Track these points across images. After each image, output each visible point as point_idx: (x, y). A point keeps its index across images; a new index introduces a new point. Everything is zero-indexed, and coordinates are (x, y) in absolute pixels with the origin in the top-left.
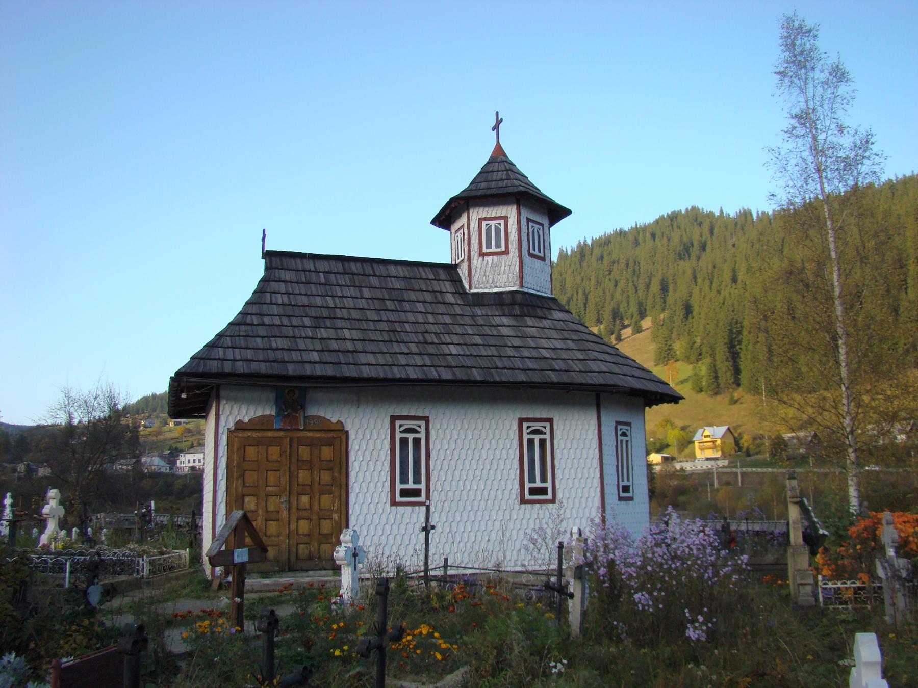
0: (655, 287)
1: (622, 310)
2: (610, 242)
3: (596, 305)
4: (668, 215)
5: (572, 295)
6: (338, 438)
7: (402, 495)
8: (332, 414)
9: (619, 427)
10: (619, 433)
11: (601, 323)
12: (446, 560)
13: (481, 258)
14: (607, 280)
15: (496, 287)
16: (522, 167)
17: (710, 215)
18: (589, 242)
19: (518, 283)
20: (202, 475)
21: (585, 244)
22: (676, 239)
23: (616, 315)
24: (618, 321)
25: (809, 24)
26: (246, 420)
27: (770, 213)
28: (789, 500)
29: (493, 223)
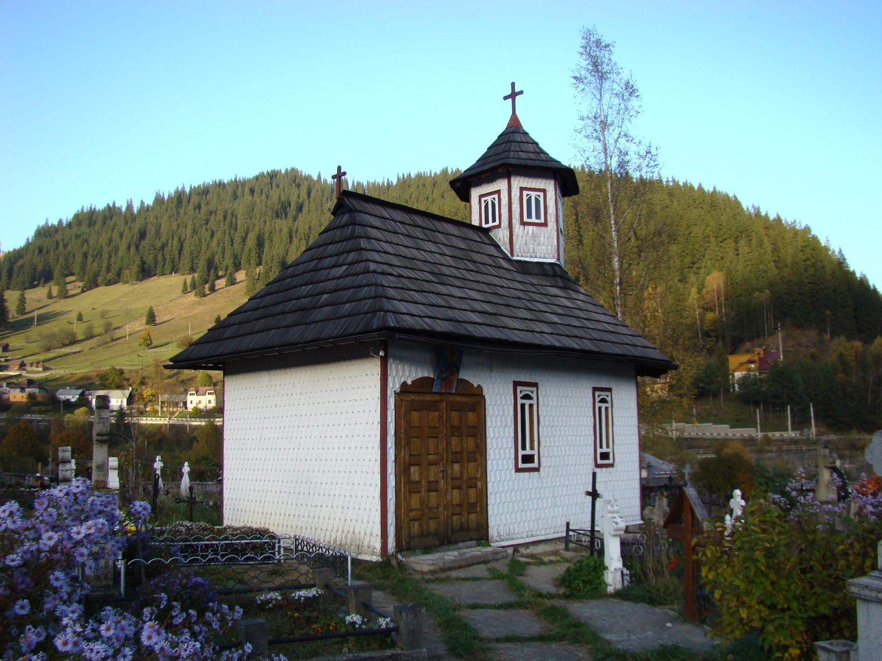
0: (251, 242)
1: (216, 261)
2: (208, 192)
3: (191, 253)
4: (268, 172)
5: (167, 241)
6: (475, 402)
7: (523, 462)
8: (473, 377)
9: (519, 389)
10: (597, 399)
11: (195, 271)
12: (568, 524)
13: (522, 227)
14: (204, 230)
15: (536, 257)
16: (534, 135)
17: (308, 178)
18: (188, 190)
19: (556, 255)
20: (222, 434)
21: (183, 192)
22: (274, 198)
23: (211, 265)
24: (212, 271)
25: (606, 40)
26: (409, 382)
27: (365, 184)
28: (95, 437)
29: (533, 194)
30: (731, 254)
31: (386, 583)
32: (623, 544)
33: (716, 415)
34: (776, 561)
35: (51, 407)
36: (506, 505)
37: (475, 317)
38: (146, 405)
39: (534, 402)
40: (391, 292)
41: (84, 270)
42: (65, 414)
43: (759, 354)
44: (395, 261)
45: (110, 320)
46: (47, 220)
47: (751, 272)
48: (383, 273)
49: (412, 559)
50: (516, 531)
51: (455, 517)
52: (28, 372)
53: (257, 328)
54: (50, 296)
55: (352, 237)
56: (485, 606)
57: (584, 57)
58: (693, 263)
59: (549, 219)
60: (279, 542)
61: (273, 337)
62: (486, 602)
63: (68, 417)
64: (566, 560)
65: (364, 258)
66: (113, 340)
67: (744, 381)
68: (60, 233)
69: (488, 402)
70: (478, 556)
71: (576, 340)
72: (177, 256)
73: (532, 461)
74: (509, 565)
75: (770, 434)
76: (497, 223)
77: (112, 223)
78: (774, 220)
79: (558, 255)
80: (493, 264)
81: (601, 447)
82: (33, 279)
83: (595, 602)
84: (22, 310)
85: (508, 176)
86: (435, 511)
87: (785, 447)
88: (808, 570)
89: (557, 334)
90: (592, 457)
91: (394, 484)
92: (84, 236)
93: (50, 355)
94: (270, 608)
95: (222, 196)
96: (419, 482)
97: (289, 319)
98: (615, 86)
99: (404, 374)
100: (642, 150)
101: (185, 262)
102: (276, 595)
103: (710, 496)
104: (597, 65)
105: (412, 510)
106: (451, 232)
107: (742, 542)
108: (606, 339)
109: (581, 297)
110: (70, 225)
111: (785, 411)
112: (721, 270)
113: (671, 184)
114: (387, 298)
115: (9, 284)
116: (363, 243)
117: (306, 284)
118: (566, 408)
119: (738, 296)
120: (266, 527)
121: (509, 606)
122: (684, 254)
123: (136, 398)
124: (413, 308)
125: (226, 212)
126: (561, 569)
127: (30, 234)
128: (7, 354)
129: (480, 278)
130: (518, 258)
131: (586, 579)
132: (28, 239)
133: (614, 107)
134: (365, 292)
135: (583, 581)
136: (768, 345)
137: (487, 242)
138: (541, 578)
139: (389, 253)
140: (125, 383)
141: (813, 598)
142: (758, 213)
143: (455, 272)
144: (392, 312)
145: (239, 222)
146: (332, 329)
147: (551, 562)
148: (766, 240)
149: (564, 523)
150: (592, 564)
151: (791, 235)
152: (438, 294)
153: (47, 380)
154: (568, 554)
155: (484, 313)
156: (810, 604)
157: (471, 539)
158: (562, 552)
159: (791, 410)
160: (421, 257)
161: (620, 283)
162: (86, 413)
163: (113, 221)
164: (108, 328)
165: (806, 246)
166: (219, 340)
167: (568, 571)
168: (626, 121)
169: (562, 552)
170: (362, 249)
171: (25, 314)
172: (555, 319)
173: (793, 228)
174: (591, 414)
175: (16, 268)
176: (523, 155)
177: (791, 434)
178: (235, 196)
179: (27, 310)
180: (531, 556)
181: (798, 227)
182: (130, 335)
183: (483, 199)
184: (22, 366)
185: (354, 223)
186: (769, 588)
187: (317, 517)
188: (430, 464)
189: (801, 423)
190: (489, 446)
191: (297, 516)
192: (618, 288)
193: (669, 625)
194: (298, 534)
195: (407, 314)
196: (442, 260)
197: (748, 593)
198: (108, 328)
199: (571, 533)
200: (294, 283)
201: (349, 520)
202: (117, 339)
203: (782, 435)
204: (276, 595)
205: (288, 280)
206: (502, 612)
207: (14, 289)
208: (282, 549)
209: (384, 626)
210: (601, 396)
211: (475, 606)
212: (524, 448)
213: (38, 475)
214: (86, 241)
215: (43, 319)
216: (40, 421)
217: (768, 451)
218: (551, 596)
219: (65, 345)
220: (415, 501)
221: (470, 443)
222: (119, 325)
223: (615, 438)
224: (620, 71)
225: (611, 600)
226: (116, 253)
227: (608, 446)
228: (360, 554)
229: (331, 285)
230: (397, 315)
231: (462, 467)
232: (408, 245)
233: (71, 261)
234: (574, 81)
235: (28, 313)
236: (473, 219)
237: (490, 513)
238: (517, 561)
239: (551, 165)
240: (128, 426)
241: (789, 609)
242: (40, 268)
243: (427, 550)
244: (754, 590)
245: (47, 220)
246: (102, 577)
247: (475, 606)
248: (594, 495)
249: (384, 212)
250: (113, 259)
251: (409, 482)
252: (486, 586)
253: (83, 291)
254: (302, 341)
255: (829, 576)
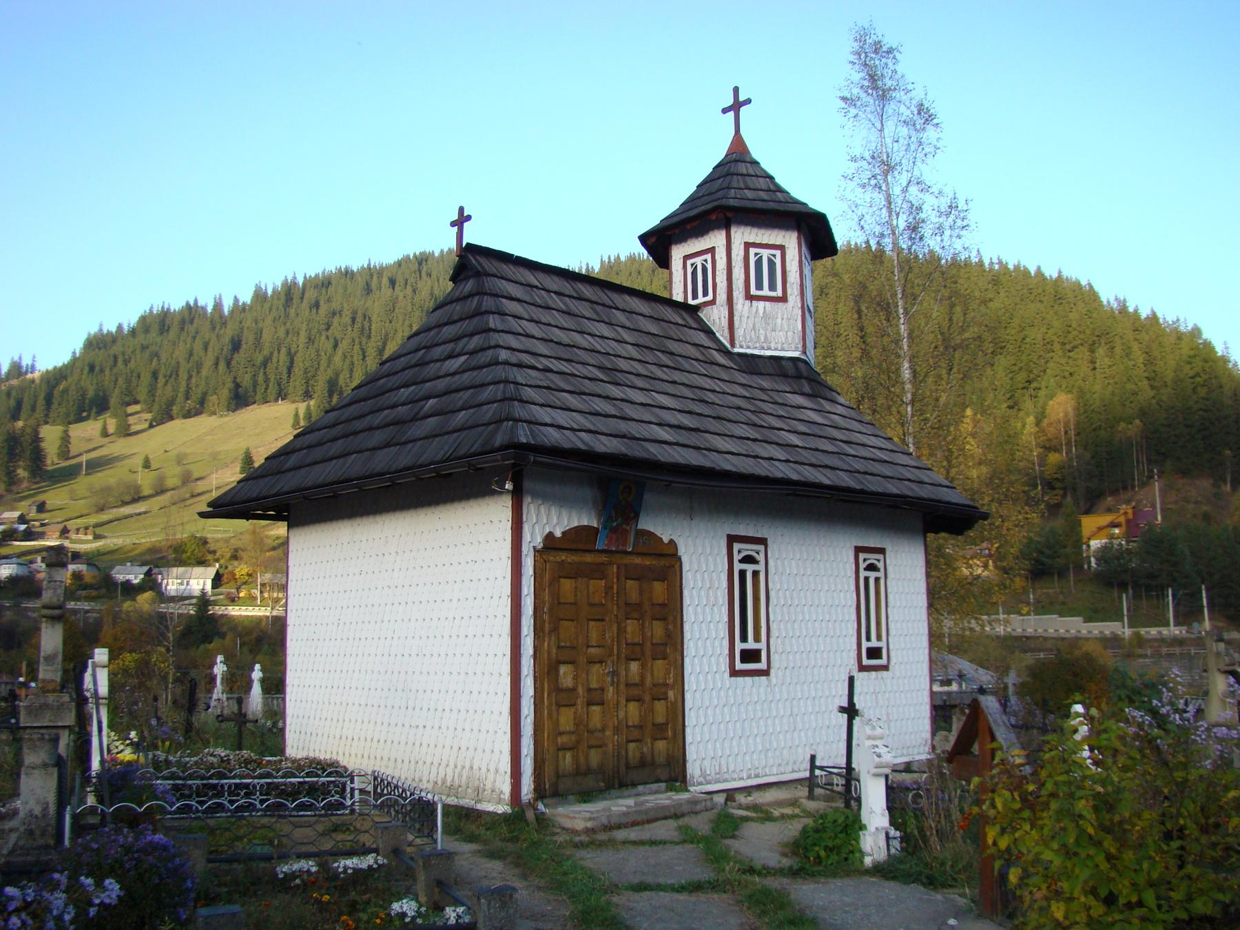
1: (341, 382)
2: (330, 283)
3: (306, 372)
4: (415, 255)
6: (666, 565)
7: (743, 661)
8: (663, 528)
10: (862, 565)
11: (311, 397)
12: (813, 758)
14: (323, 338)
15: (769, 349)
18: (300, 281)
19: (800, 346)
21: (295, 283)
26: (558, 534)
29: (765, 253)
30: (1085, 368)
31: (511, 847)
32: (890, 789)
33: (1063, 603)
34: (1117, 818)
35: (103, 591)
36: (714, 727)
37: (663, 434)
38: (238, 589)
39: (760, 567)
40: (530, 393)
41: (153, 395)
42: (124, 601)
43: (1126, 513)
44: (542, 348)
45: (190, 467)
46: (101, 325)
47: (1113, 394)
48: (520, 365)
49: (561, 810)
50: (731, 769)
51: (632, 746)
52: (73, 542)
53: (331, 453)
54: (105, 434)
55: (479, 313)
56: (659, 887)
57: (857, 67)
58: (1029, 382)
59: (789, 291)
60: (352, 782)
61: (353, 466)
62: (662, 880)
63: (127, 605)
64: (808, 814)
65: (492, 343)
66: (193, 496)
67: (1104, 555)
68: (119, 343)
69: (686, 567)
70: (664, 807)
71: (827, 472)
72: (285, 376)
73: (758, 660)
74: (712, 821)
75: (1143, 631)
76: (710, 297)
77: (192, 329)
78: (1147, 318)
79: (804, 346)
80: (701, 358)
81: (868, 639)
82: (81, 409)
83: (839, 882)
84: (65, 453)
85: (726, 225)
86: (599, 735)
87: (1164, 650)
88: (1175, 834)
89: (795, 462)
90: (854, 654)
91: (531, 692)
92: (153, 348)
93: (104, 517)
94: (297, 886)
95: (350, 290)
96: (574, 690)
97: (378, 437)
98: (902, 109)
99: (549, 520)
100: (944, 203)
101: (297, 383)
102: (310, 865)
103: (1044, 718)
104: (875, 76)
105: (561, 734)
106: (637, 310)
107: (1056, 783)
108: (875, 471)
109: (840, 410)
110: (133, 332)
111: (1165, 596)
112: (1070, 392)
113: (997, 267)
114: (521, 401)
115: (47, 416)
116: (493, 321)
117: (406, 385)
118: (811, 577)
119: (1095, 430)
120: (334, 757)
121: (696, 887)
122: (1016, 368)
123: (225, 579)
124: (562, 418)
125: (355, 313)
126: (793, 829)
127: (77, 345)
128: (43, 516)
129: (677, 376)
130: (741, 351)
131: (830, 844)
132: (74, 353)
133: (901, 140)
134: (488, 392)
135: (826, 848)
136: (1139, 502)
137: (694, 325)
138: (762, 843)
139: (533, 337)
140: (210, 557)
141: (1184, 886)
142: (1123, 309)
143: (639, 368)
144: (526, 421)
145: (373, 327)
146: (436, 450)
147: (783, 817)
148: (1135, 347)
149: (808, 757)
150: (841, 820)
151: (1172, 339)
152: (607, 397)
153: (99, 553)
154: (811, 805)
155: (679, 427)
156: (1176, 896)
157: (658, 781)
158: (804, 801)
159: (1174, 595)
160: (585, 345)
161: (913, 402)
162: (153, 601)
163: (195, 325)
164: (187, 479)
165: (1195, 356)
166: (279, 472)
167: (804, 830)
168: (918, 163)
169: (804, 801)
170: (490, 330)
171: (68, 459)
172: (794, 439)
173: (1176, 330)
174: (853, 588)
175: (56, 393)
176: (749, 194)
177: (1174, 631)
178: (368, 290)
179: (71, 454)
180: (754, 807)
181: (1182, 328)
182: (217, 488)
183: (689, 262)
184: (64, 532)
185: (480, 293)
186: (1104, 866)
187: (417, 744)
188: (591, 662)
189: (1188, 614)
190: (687, 635)
191: (389, 742)
192: (909, 409)
193: (952, 922)
194: (377, 768)
195: (552, 425)
196: (619, 349)
197: (1069, 876)
198: (187, 479)
199: (817, 772)
200: (390, 384)
201: (464, 749)
202: (199, 494)
203: (1160, 633)
204: (310, 865)
205: (382, 381)
206: (682, 897)
207: (54, 423)
208: (357, 792)
209: (452, 921)
210: (869, 565)
211: (641, 887)
212: (744, 638)
213: (21, 679)
214: (157, 355)
215: (95, 466)
216: (87, 612)
217: (1140, 656)
218: (766, 871)
219: (124, 503)
220: (566, 719)
221: (658, 630)
222: (202, 474)
223: (891, 626)
224: (910, 87)
225: (867, 878)
226: (198, 372)
227: (879, 638)
228: (479, 801)
229: (441, 384)
230: (534, 427)
231: (643, 666)
232: (566, 325)
233: (134, 383)
234: (843, 105)
235: (74, 457)
236: (674, 292)
237: (689, 739)
238: (729, 813)
239: (790, 207)
240: (214, 619)
241: (1140, 904)
242: (91, 393)
243: (586, 796)
244: (1077, 871)
245: (101, 325)
246: (38, 832)
247: (641, 887)
248: (851, 711)
249: (530, 277)
250: (194, 380)
251: (557, 689)
252: (667, 855)
253: (151, 426)
254: (393, 469)
255: (1214, 846)
